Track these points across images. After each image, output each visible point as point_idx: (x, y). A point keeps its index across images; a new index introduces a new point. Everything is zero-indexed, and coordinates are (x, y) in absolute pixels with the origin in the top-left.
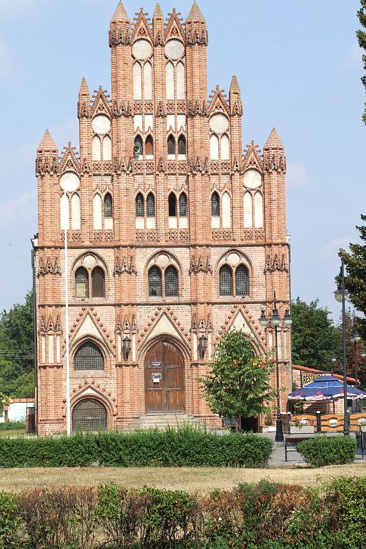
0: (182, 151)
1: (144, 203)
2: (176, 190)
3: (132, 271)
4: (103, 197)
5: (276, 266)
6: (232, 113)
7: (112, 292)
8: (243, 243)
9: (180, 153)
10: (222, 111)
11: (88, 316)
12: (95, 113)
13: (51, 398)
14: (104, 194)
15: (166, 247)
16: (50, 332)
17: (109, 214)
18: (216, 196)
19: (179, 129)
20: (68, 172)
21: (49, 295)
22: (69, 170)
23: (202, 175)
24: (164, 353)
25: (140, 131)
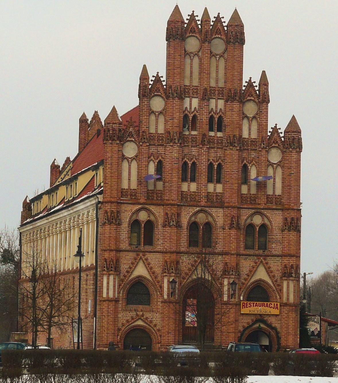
0: (219, 130)
2: (214, 161)
11: (141, 261)
15: (205, 207)
25: (188, 111)
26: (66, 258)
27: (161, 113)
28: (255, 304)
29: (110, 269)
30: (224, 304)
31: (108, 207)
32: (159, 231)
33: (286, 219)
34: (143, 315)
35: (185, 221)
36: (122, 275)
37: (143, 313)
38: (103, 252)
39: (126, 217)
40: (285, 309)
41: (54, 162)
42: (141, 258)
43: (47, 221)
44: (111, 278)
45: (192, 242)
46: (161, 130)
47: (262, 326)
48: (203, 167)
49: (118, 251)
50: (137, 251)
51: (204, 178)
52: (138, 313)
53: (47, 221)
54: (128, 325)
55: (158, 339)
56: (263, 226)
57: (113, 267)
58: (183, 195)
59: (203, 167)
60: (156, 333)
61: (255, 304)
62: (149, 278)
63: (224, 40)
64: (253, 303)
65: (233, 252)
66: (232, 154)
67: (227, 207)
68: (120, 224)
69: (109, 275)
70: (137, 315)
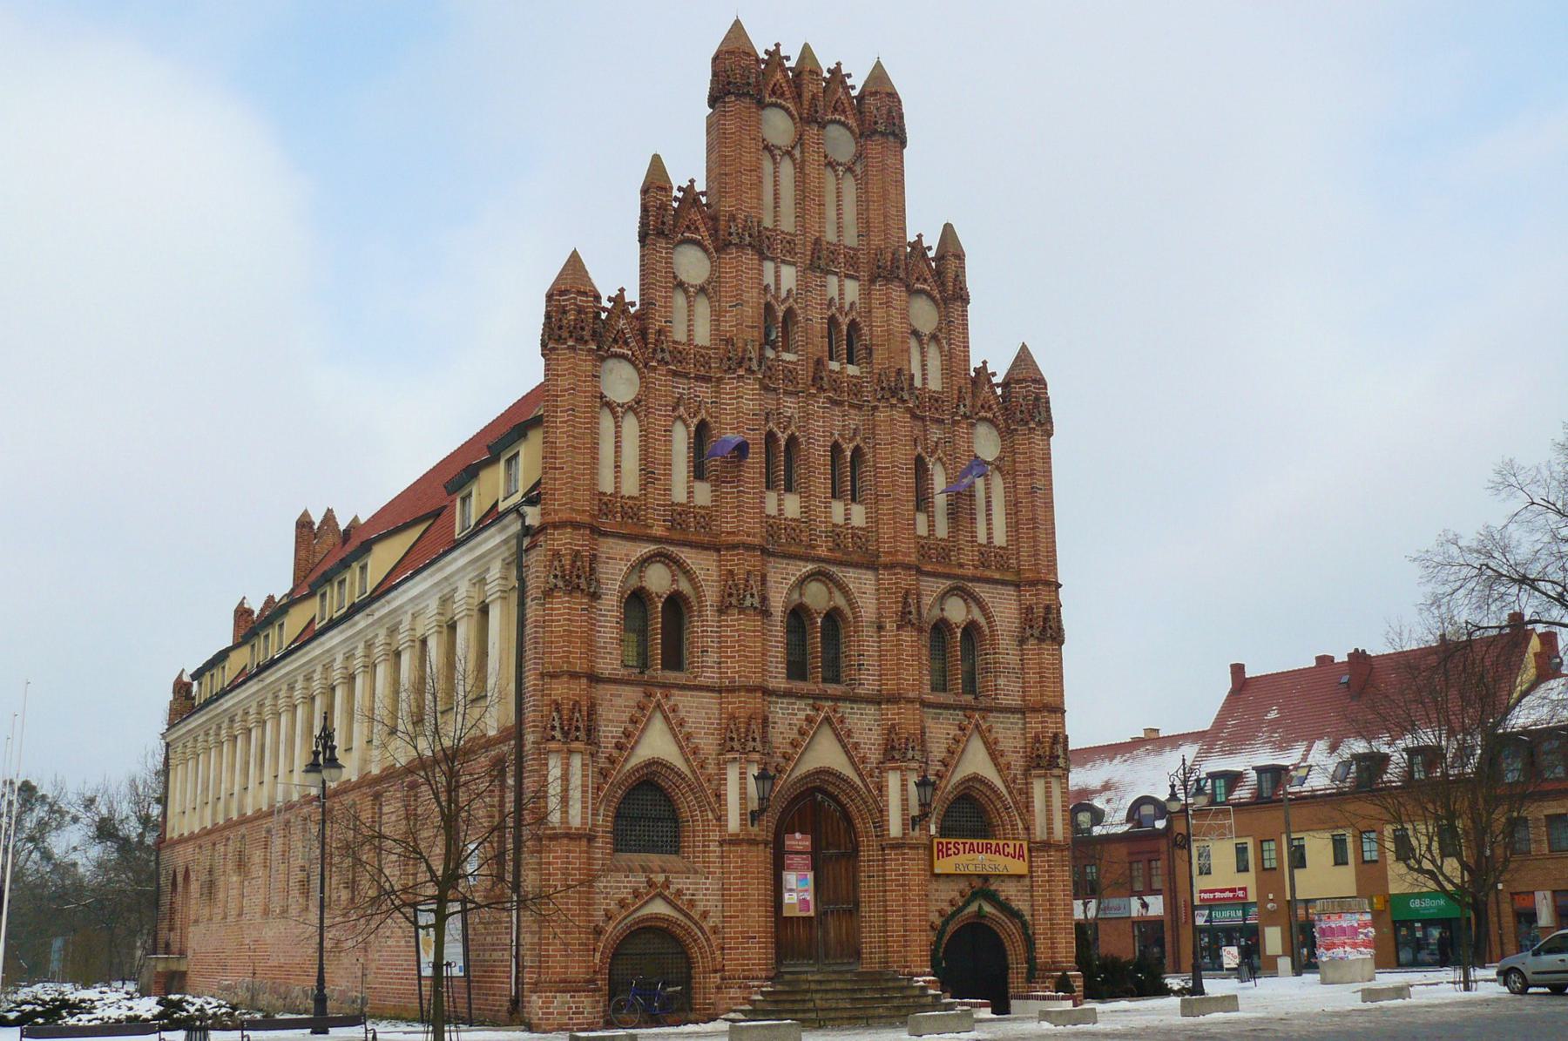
11: (658, 715)
27: (702, 290)
29: (573, 734)
30: (893, 847)
31: (563, 540)
32: (705, 627)
33: (1030, 609)
34: (667, 884)
35: (778, 603)
38: (547, 680)
39: (614, 574)
40: (1040, 861)
41: (242, 603)
42: (659, 706)
43: (261, 685)
44: (576, 761)
46: (703, 335)
47: (988, 908)
48: (818, 453)
49: (594, 678)
50: (647, 684)
51: (821, 484)
53: (261, 685)
55: (714, 959)
56: (971, 629)
57: (577, 727)
58: (773, 527)
59: (818, 453)
60: (708, 940)
62: (684, 768)
63: (852, 132)
65: (911, 695)
66: (893, 422)
67: (890, 567)
68: (595, 596)
69: (570, 752)
70: (651, 884)
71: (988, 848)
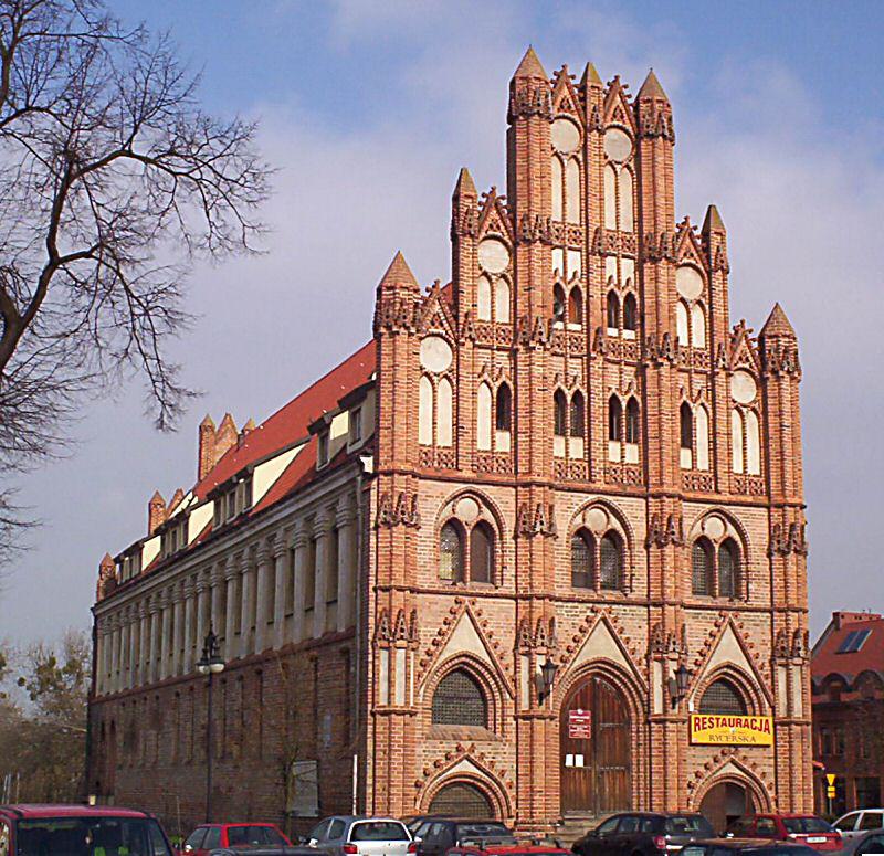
1: (571, 413)
3: (550, 534)
4: (495, 390)
5: (787, 542)
6: (711, 264)
7: (510, 573)
8: (733, 498)
9: (626, 328)
10: (693, 262)
11: (466, 614)
12: (483, 234)
13: (397, 778)
14: (498, 384)
15: (606, 493)
16: (399, 643)
17: (503, 418)
18: (685, 411)
19: (623, 283)
20: (433, 335)
21: (398, 569)
22: (435, 331)
23: (545, 350)
24: (595, 697)
26: (253, 628)
28: (721, 721)
36: (422, 650)
37: (473, 745)
45: (584, 578)
51: (600, 429)
52: (461, 743)
54: (439, 775)
61: (721, 721)
64: (718, 719)
70: (459, 749)
71: (738, 723)
